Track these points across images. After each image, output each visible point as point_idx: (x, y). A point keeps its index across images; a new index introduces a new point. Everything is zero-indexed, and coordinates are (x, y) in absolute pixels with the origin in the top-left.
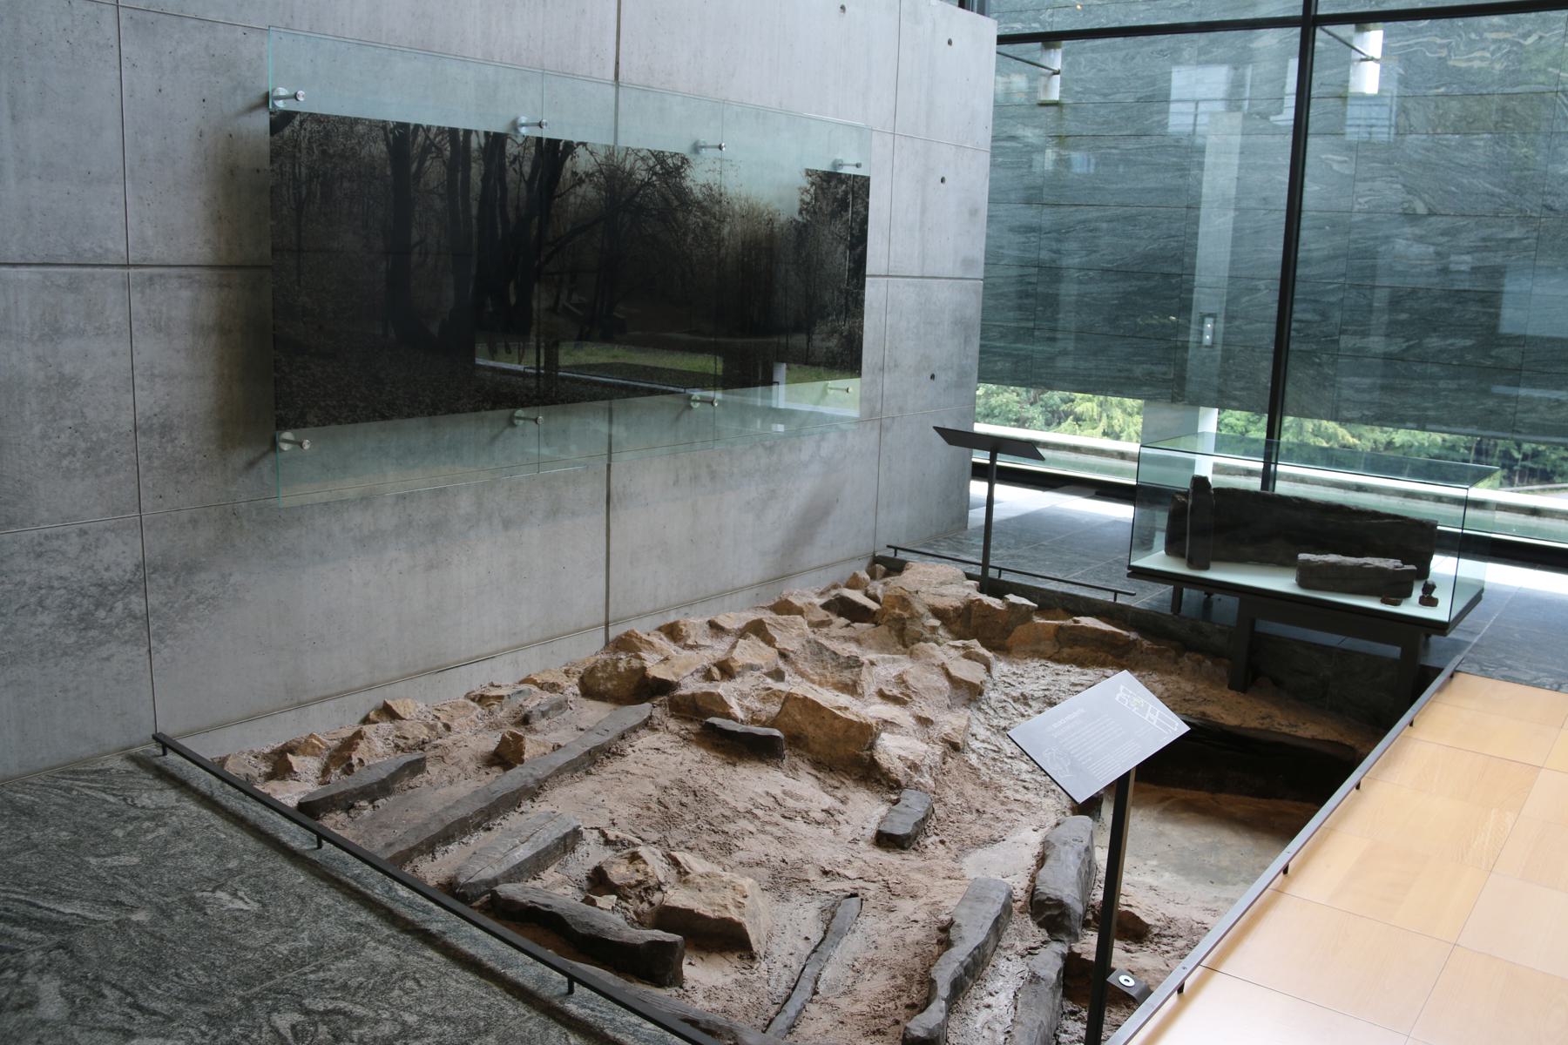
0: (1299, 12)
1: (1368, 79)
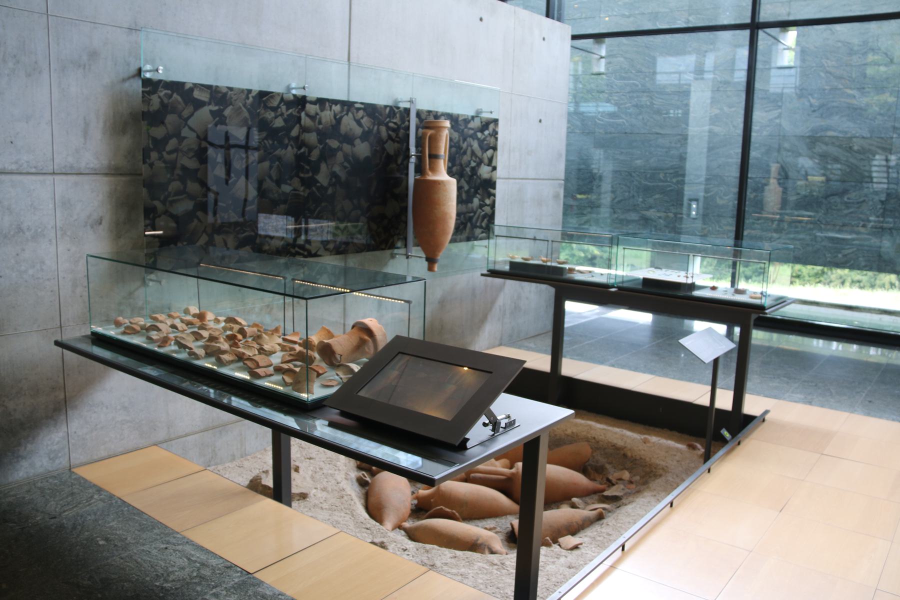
0: (748, 21)
1: (788, 58)
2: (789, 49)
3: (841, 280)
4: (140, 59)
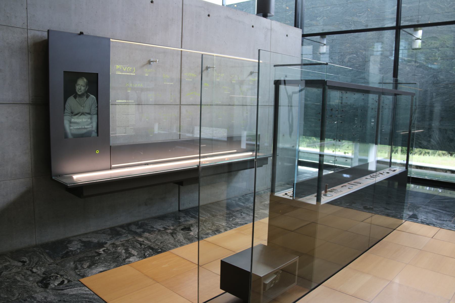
2: (418, 39)
3: (420, 152)
4: (309, 72)
